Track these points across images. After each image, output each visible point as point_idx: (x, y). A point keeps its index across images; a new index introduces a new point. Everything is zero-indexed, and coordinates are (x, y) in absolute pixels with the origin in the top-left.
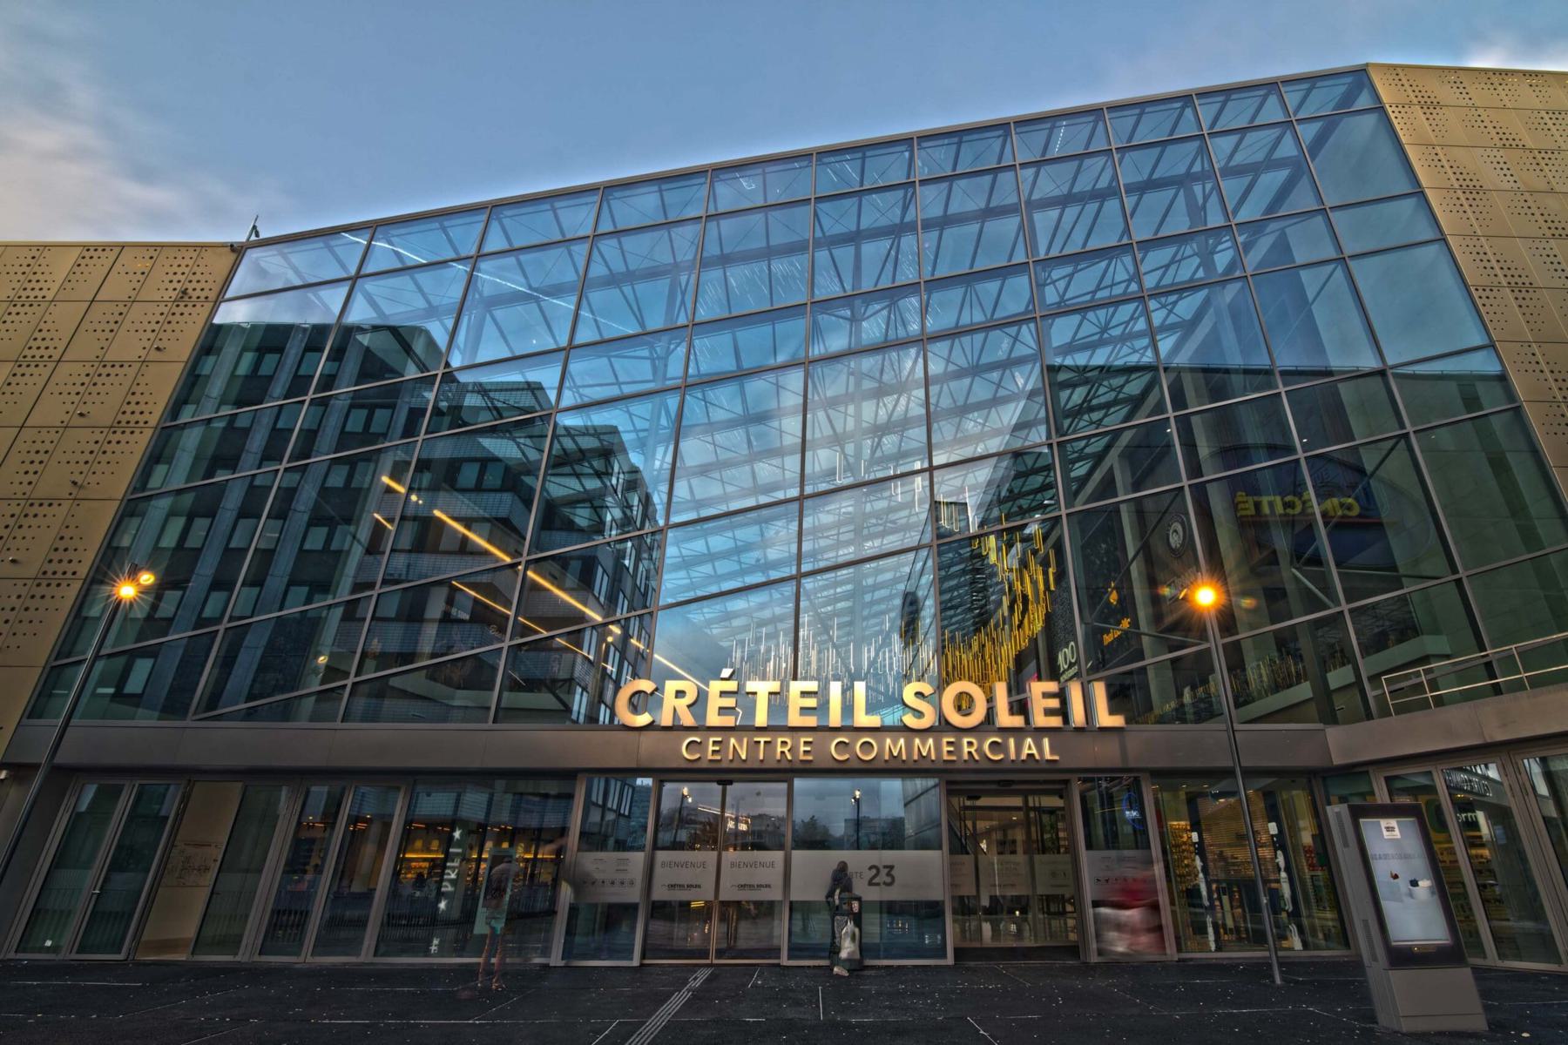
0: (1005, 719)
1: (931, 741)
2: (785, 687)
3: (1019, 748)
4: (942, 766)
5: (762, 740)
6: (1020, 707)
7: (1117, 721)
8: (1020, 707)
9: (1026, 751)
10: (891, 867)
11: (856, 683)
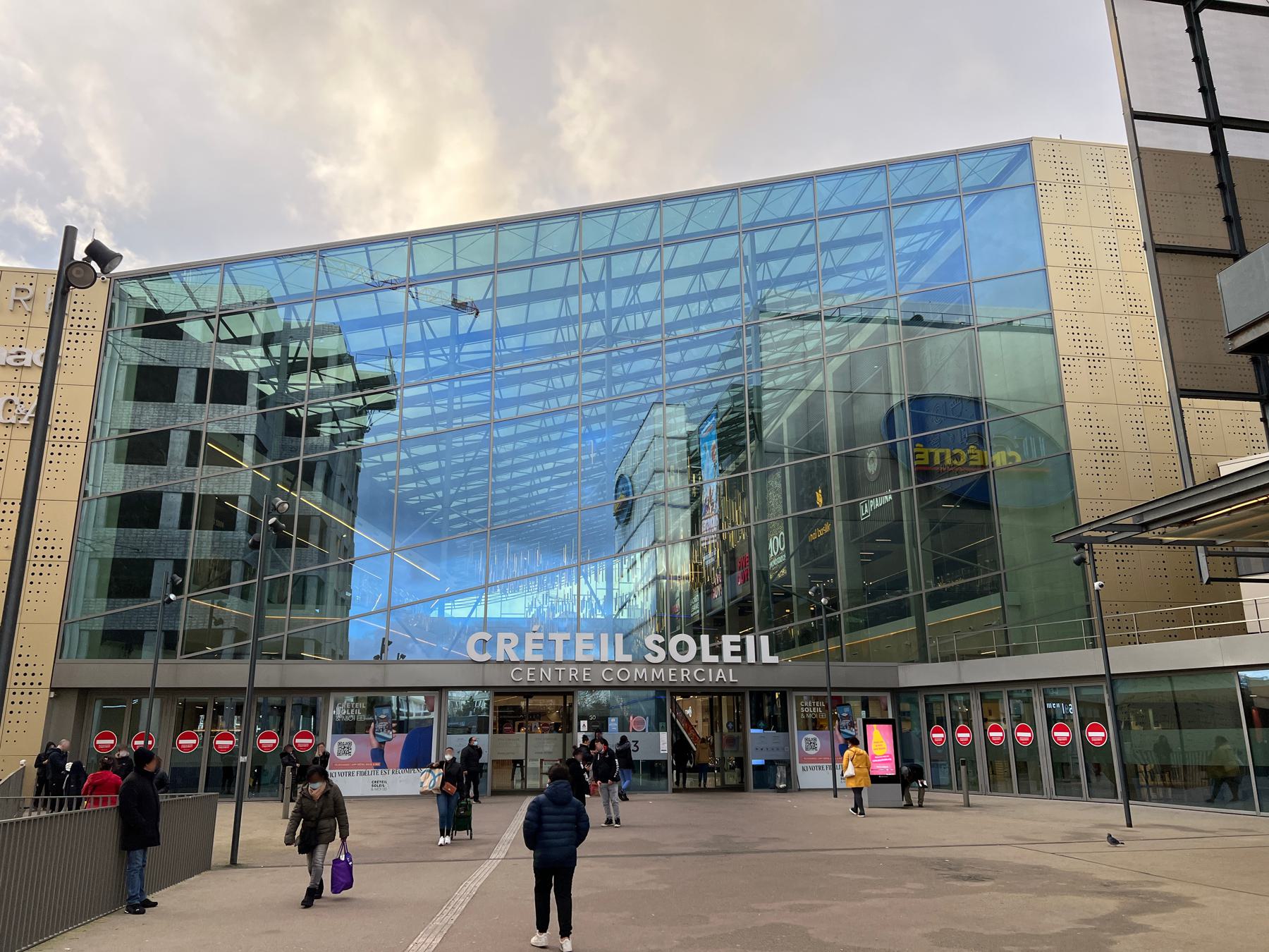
0: (707, 657)
1: (662, 670)
2: (574, 638)
3: (714, 677)
4: (526, 684)
5: (560, 669)
6: (716, 650)
7: (775, 659)
8: (716, 650)
9: (718, 677)
10: (637, 742)
11: (602, 635)
